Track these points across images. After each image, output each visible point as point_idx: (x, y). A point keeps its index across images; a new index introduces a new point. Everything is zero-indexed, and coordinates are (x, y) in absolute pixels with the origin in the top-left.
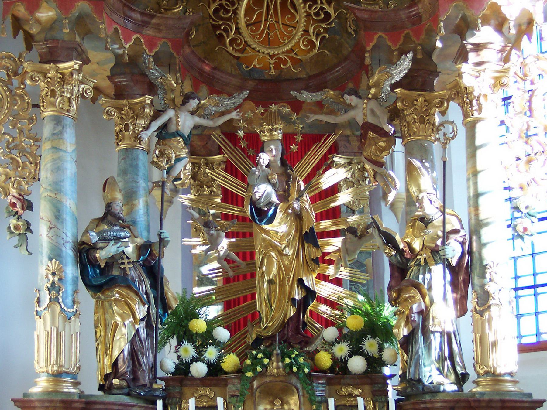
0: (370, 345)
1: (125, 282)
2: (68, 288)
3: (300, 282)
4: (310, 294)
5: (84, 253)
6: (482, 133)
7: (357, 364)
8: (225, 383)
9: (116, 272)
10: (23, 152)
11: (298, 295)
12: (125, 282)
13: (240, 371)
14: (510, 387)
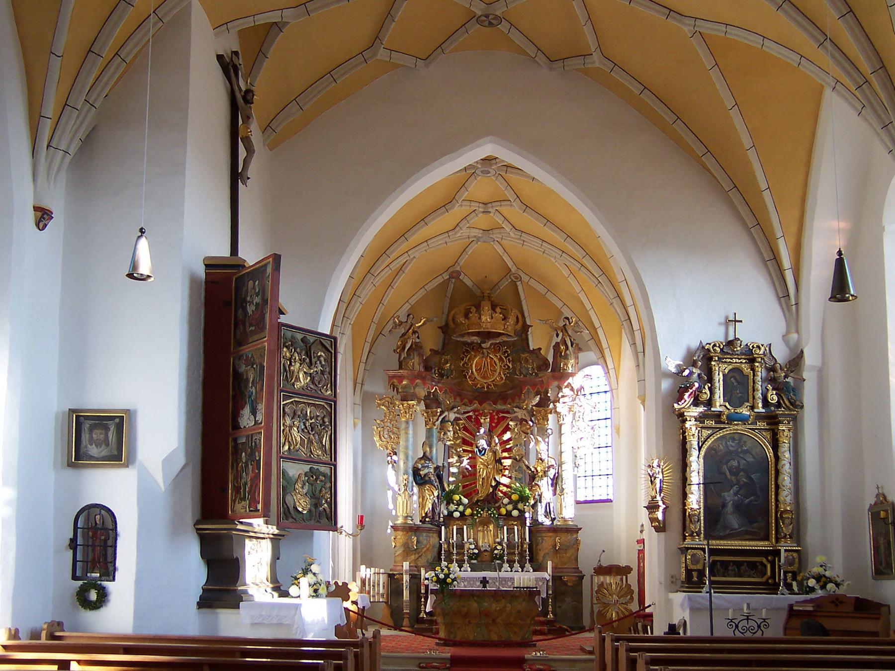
0: (520, 506)
1: (430, 482)
2: (410, 485)
3: (495, 479)
4: (498, 483)
5: (416, 472)
6: (564, 429)
7: (515, 513)
8: (466, 520)
9: (427, 478)
10: (393, 433)
11: (494, 484)
12: (430, 482)
13: (472, 515)
14: (570, 523)
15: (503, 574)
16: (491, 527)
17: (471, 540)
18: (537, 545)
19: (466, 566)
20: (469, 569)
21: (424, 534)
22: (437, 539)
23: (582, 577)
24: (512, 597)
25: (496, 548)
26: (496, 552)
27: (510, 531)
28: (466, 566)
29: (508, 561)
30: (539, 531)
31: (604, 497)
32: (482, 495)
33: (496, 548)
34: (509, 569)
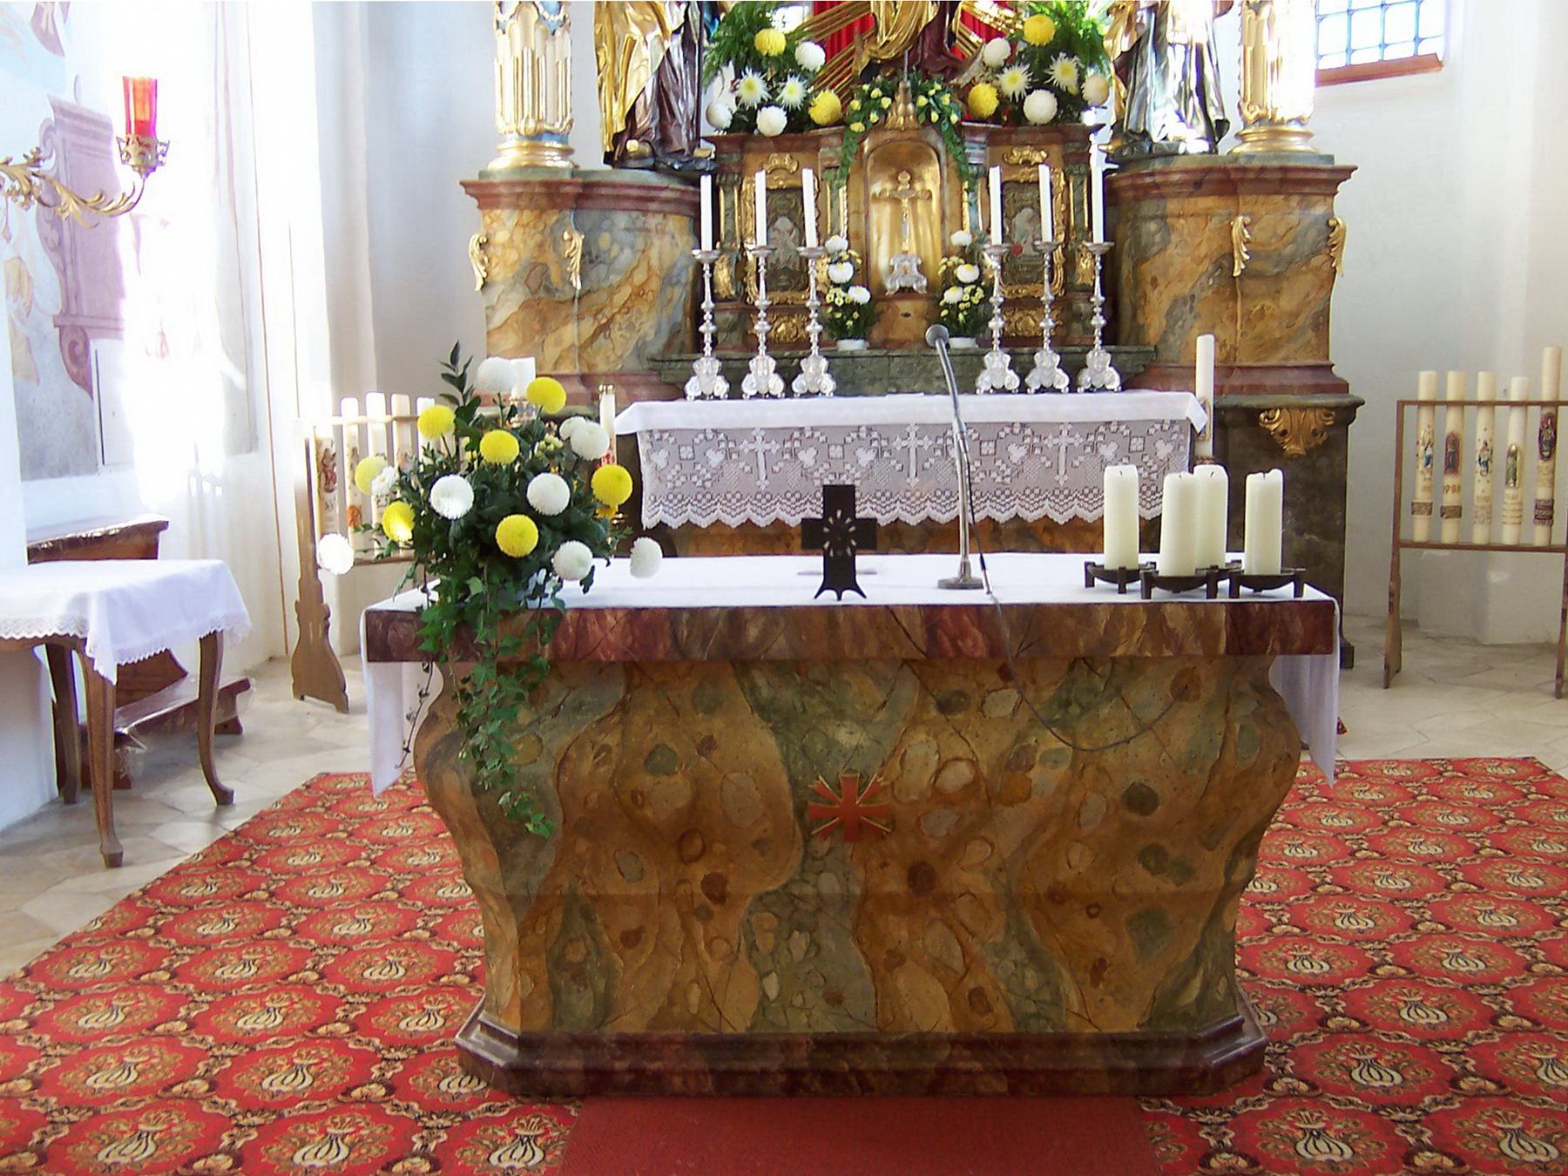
0: (1063, 70)
7: (1040, 106)
8: (816, 145)
13: (841, 122)
14: (1297, 144)
15: (979, 407)
16: (931, 177)
17: (838, 243)
18: (1141, 258)
19: (815, 369)
20: (828, 384)
21: (622, 219)
22: (684, 240)
23: (1347, 413)
24: (1087, 662)
25: (950, 280)
26: (952, 295)
27: (1019, 193)
28: (815, 369)
29: (1007, 341)
30: (1156, 191)
31: (1401, 51)
32: (889, 38)
33: (950, 280)
34: (1012, 380)
